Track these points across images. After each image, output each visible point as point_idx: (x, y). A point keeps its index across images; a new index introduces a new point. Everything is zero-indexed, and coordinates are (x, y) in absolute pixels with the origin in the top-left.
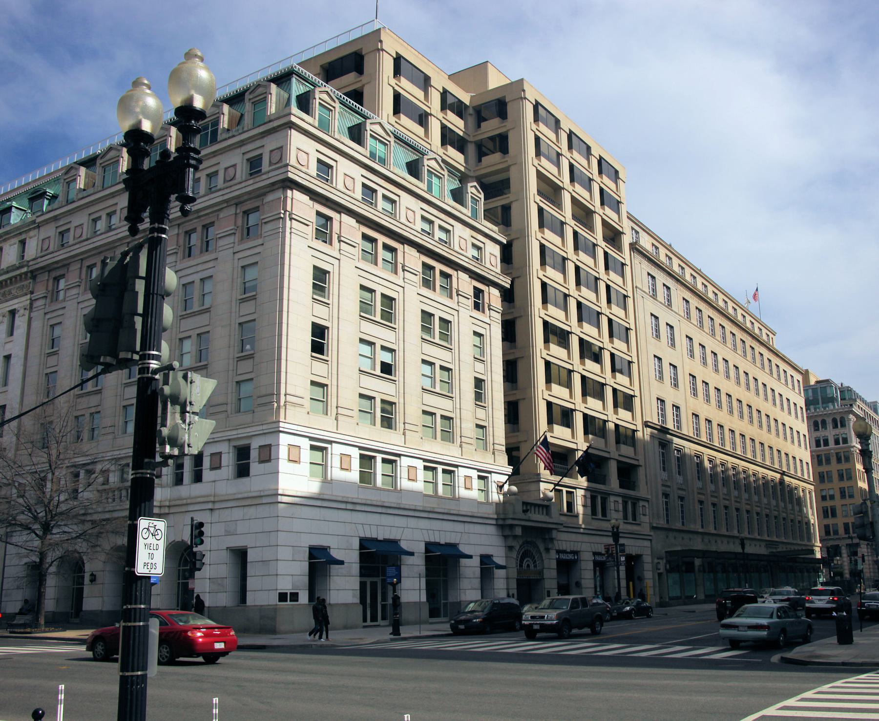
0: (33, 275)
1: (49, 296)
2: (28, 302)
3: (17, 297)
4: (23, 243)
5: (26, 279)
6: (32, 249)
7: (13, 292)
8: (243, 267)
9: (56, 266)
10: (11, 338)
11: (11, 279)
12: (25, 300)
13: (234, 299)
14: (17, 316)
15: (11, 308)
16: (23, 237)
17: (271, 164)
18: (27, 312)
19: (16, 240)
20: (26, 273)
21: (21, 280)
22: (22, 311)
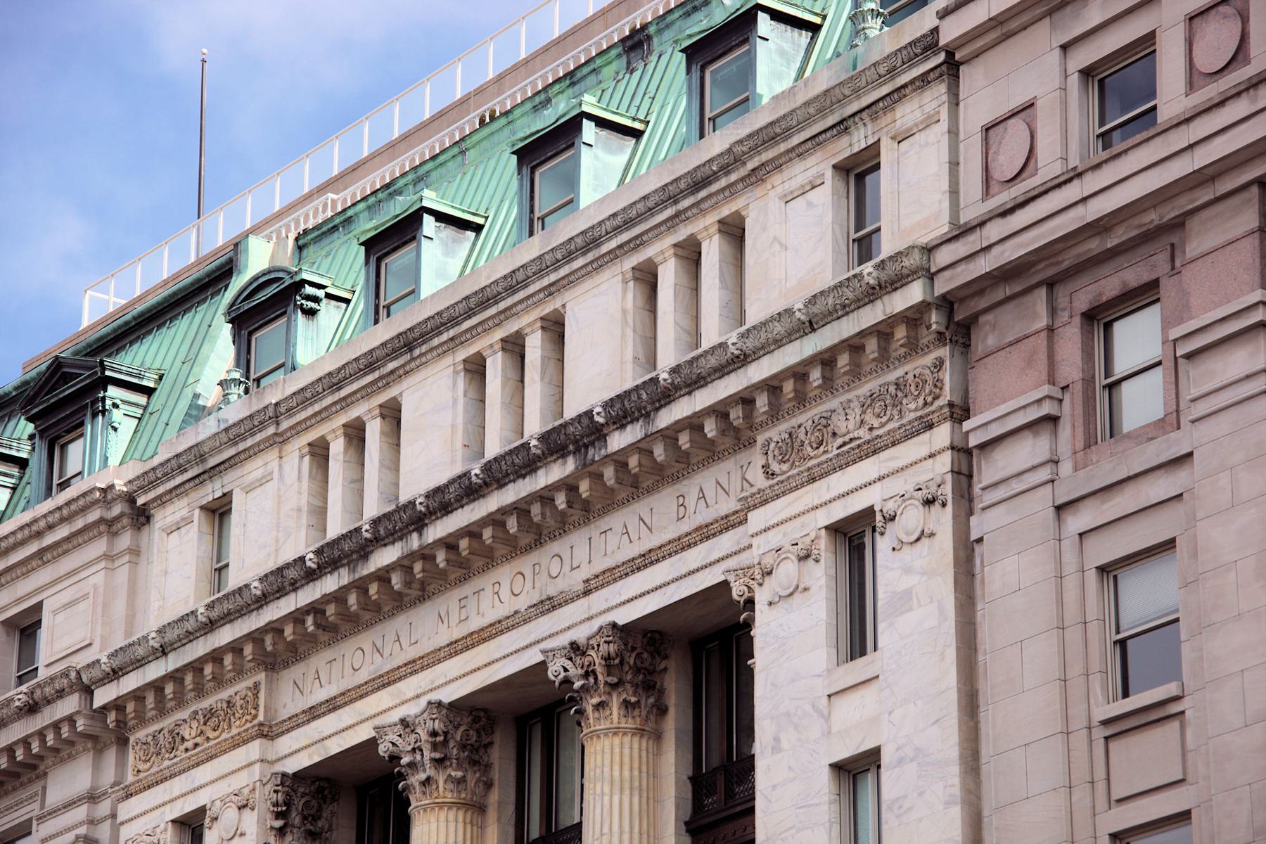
0: (958, 320)
1: (1070, 410)
2: (945, 462)
3: (871, 449)
4: (859, 172)
5: (913, 347)
6: (915, 198)
7: (845, 425)
8: (1106, 570)
9: (1094, 246)
10: (861, 669)
11: (826, 359)
12: (926, 458)
13: (1078, 723)
14: (883, 544)
15: (839, 512)
16: (858, 140)
17: (1194, 77)
18: (943, 521)
19: (820, 165)
20: (913, 318)
21: (884, 359)
22: (912, 518)
